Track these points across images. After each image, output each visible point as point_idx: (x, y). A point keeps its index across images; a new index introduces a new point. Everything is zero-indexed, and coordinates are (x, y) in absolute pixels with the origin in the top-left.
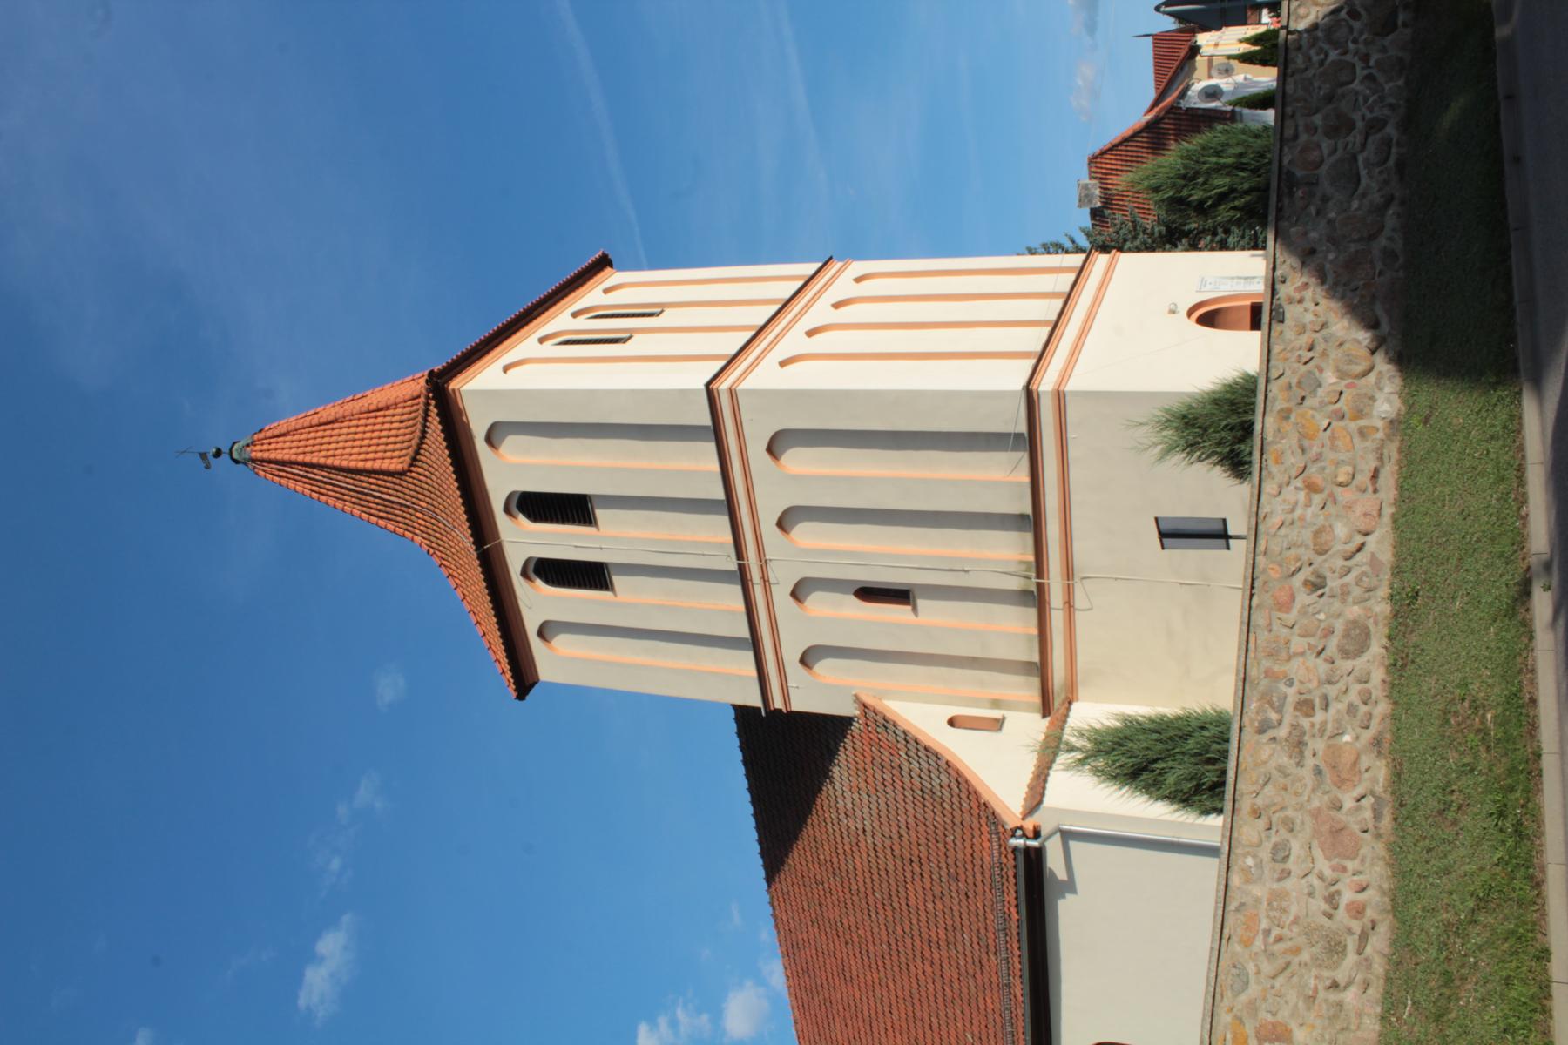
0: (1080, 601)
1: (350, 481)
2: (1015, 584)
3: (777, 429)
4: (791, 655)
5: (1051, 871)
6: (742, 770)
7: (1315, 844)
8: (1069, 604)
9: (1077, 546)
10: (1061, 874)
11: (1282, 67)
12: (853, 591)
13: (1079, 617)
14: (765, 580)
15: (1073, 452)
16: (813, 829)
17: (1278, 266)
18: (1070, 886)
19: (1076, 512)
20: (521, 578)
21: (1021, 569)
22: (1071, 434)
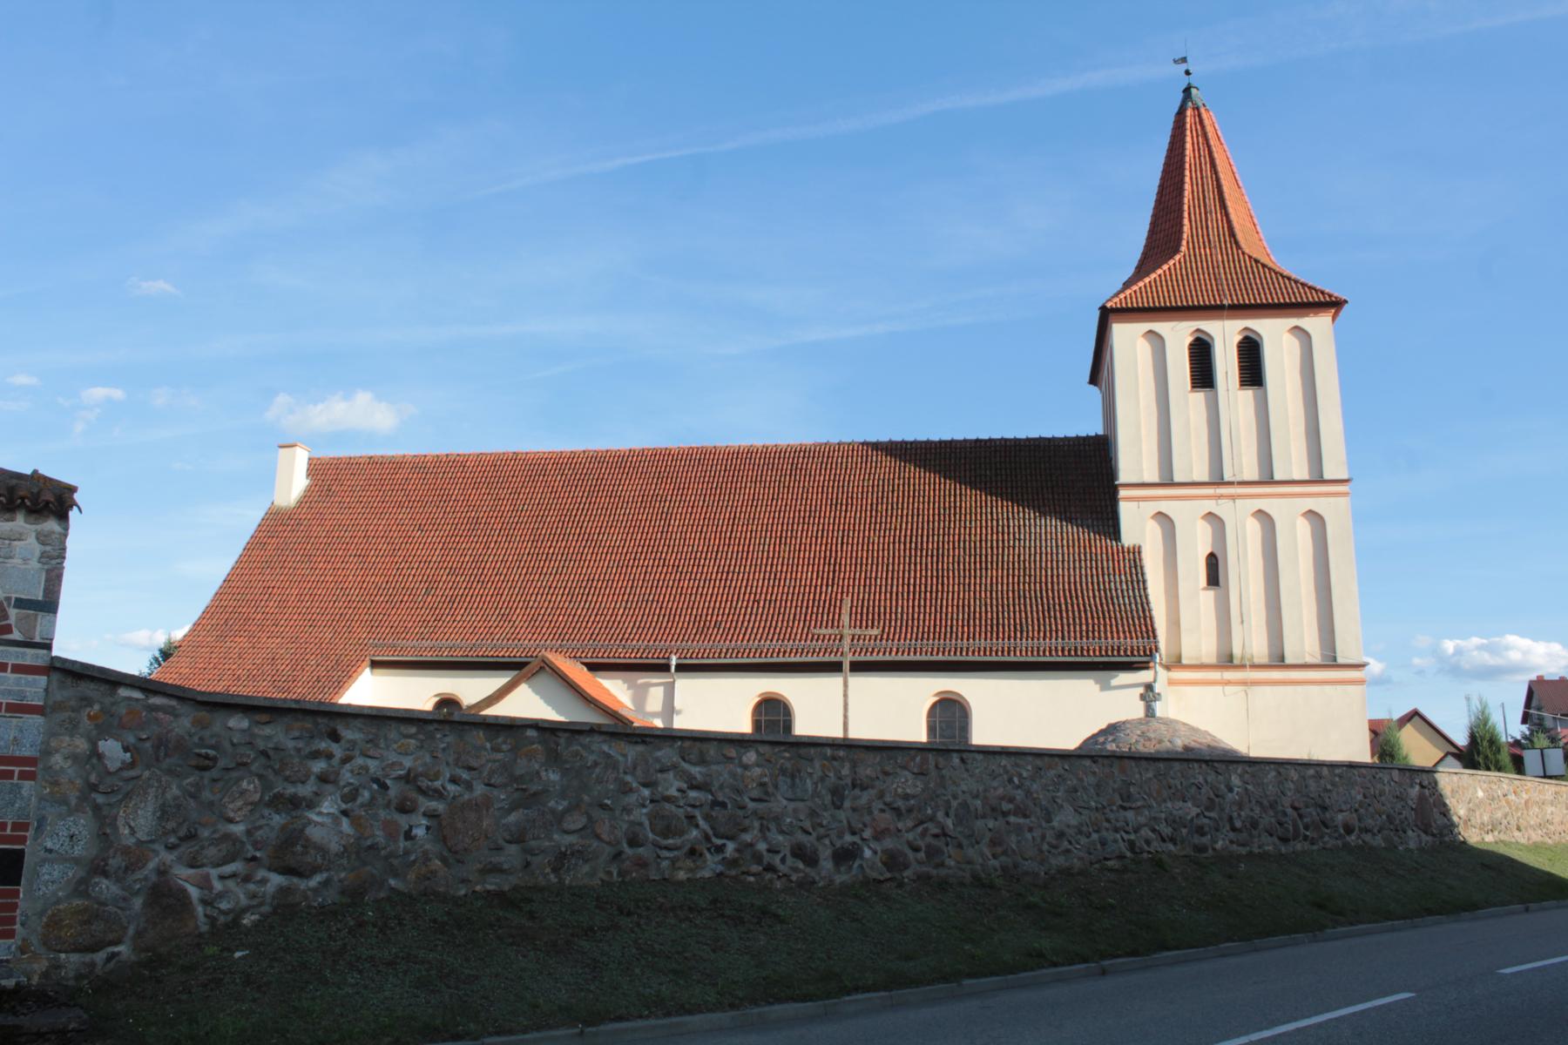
0: (1229, 689)
1: (1211, 195)
2: (1237, 651)
3: (1326, 519)
4: (1164, 506)
5: (1117, 676)
6: (947, 437)
7: (352, 787)
8: (1229, 683)
9: (1268, 689)
10: (1114, 682)
11: (752, 738)
12: (1216, 552)
13: (1219, 688)
14: (1220, 497)
15: (1328, 688)
16: (971, 498)
17: (819, 749)
18: (1106, 687)
19: (1290, 689)
20: (1195, 328)
21: (1248, 656)
22: (1339, 687)
